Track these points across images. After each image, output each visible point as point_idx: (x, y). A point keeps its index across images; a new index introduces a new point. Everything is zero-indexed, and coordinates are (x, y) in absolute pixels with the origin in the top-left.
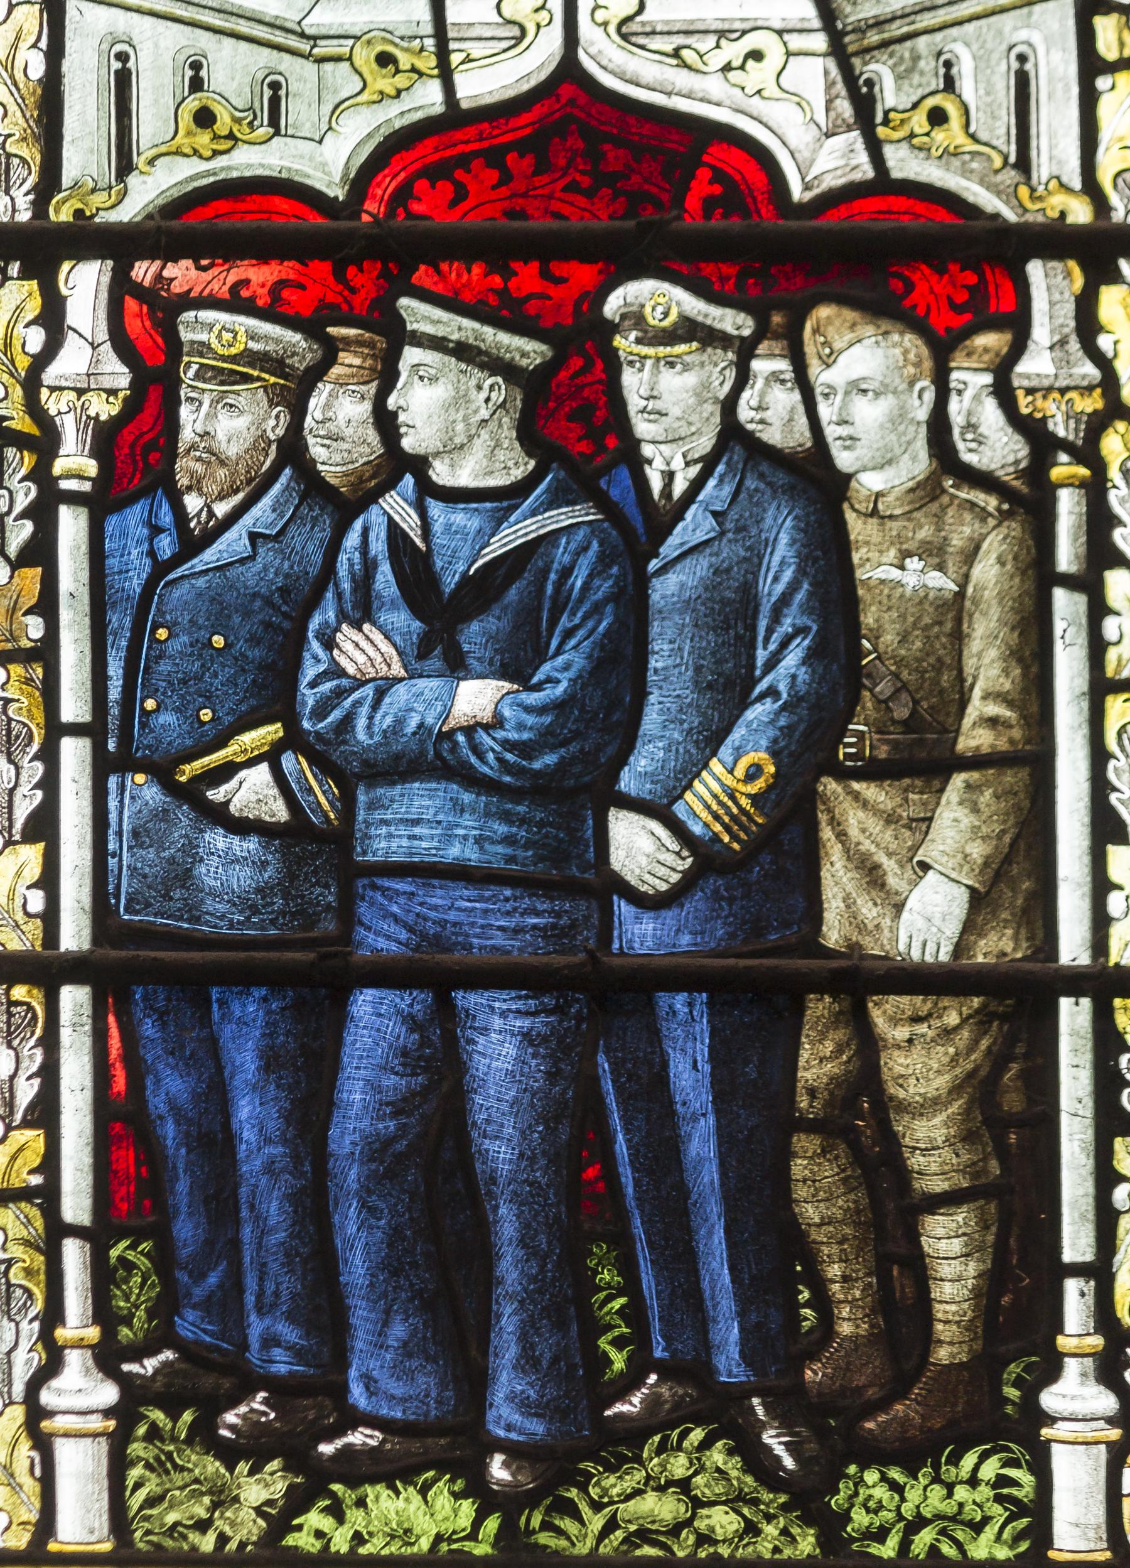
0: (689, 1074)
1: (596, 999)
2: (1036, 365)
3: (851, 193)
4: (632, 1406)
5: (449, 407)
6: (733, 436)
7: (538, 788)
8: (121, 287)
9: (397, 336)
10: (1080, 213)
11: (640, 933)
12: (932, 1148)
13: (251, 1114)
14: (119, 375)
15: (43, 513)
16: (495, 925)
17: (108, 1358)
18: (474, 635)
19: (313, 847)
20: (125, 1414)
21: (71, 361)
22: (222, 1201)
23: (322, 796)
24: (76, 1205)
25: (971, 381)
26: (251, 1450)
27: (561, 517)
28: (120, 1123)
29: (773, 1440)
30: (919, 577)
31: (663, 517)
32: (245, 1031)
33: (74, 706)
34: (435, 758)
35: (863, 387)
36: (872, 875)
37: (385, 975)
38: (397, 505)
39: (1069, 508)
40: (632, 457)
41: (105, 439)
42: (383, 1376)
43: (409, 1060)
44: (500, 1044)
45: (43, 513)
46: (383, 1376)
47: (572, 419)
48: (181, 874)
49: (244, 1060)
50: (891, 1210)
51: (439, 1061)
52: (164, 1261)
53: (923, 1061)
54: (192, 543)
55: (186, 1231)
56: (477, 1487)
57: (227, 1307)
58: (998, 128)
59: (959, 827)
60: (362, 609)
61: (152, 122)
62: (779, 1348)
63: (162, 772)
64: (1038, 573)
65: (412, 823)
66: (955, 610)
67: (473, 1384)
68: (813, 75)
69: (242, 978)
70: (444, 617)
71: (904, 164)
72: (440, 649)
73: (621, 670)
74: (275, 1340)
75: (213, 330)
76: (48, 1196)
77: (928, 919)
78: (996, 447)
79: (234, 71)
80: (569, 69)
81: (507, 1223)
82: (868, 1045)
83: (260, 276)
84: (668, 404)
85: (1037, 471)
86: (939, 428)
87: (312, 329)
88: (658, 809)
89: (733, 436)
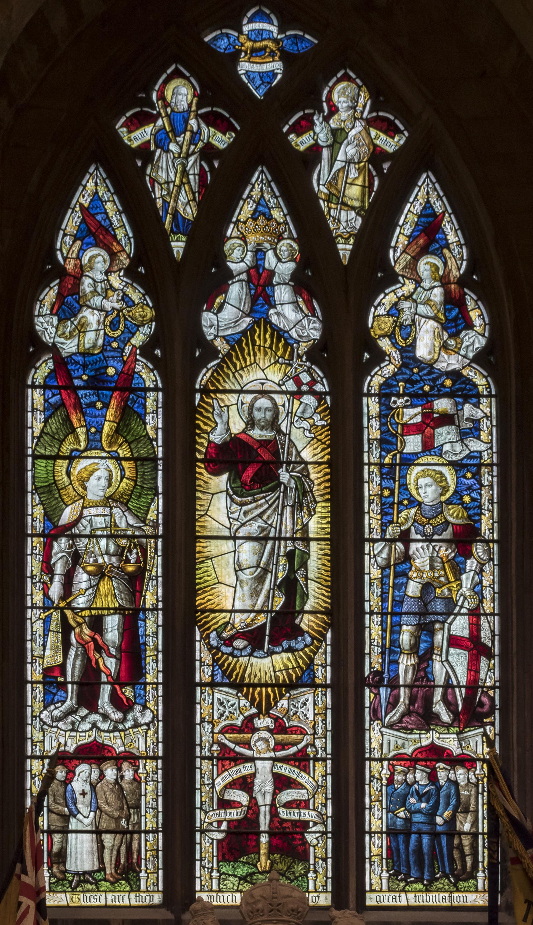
0: (444, 842)
1: (435, 835)
2: (478, 772)
3: (460, 755)
4: (438, 876)
5: (420, 776)
6: (449, 779)
7: (429, 814)
8: (389, 764)
9: (415, 769)
10: (482, 757)
11: (439, 829)
12: (467, 850)
13: (402, 847)
14: (389, 773)
15: (381, 787)
16: (425, 828)
17: (387, 871)
18: (423, 799)
19: (408, 820)
20: (389, 877)
21: (384, 771)
22: (399, 856)
23: (408, 815)
24: (384, 856)
25: (471, 773)
26: (402, 880)
27: (432, 787)
28: (389, 848)
29: (452, 879)
30: (466, 793)
31: (441, 787)
32: (401, 838)
33: (384, 806)
34: (419, 811)
35: (461, 774)
36: (461, 823)
37: (415, 833)
38: (416, 786)
39: (480, 786)
40: (439, 781)
41: (388, 779)
42: (414, 873)
43: (417, 841)
44: (426, 840)
45: (381, 787)
46: (414, 873)
47: (433, 777)
48: (395, 823)
49: (401, 841)
50: (463, 856)
51: (420, 842)
52: (393, 862)
53: (466, 841)
54: (396, 790)
55: (395, 859)
56: (423, 884)
57: (399, 866)
58: (474, 748)
59: (469, 818)
60: (412, 796)
61: (392, 748)
62: (452, 870)
63: (393, 813)
64: (477, 793)
65: (417, 818)
66: (470, 796)
67: (423, 874)
68: (456, 743)
69: (401, 833)
70: (420, 797)
71: (465, 752)
72: (420, 800)
73: (437, 802)
74: (403, 869)
75: (399, 768)
76: (382, 855)
77: (467, 827)
78: (473, 780)
79: (400, 742)
80: (95, 740)
81: (426, 857)
82: (461, 840)
83: (403, 763)
84: (442, 775)
85: (478, 783)
86: (468, 778)
87: (408, 768)
88: (441, 816)
89: (449, 779)
